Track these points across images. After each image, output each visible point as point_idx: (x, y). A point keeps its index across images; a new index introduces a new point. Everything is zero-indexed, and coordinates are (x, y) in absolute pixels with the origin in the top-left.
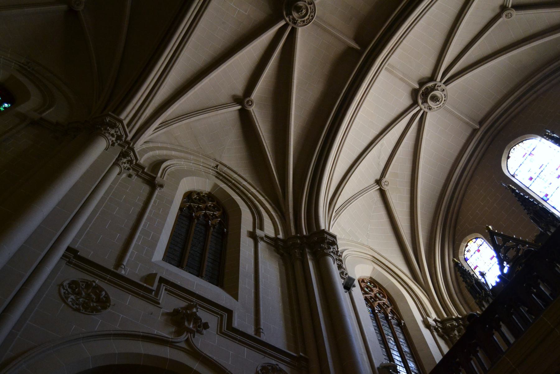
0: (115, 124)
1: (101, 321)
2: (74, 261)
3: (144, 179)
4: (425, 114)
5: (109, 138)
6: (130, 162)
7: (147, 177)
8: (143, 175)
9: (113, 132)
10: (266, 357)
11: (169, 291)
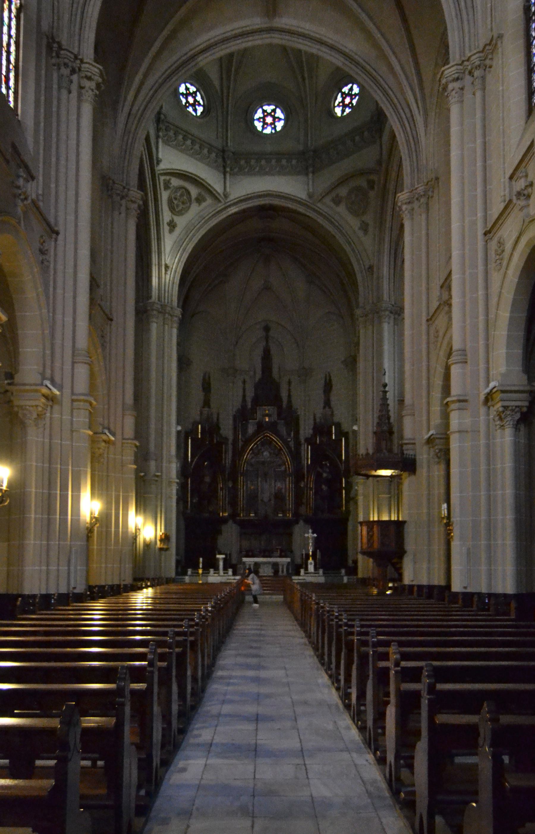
2: (491, 235)
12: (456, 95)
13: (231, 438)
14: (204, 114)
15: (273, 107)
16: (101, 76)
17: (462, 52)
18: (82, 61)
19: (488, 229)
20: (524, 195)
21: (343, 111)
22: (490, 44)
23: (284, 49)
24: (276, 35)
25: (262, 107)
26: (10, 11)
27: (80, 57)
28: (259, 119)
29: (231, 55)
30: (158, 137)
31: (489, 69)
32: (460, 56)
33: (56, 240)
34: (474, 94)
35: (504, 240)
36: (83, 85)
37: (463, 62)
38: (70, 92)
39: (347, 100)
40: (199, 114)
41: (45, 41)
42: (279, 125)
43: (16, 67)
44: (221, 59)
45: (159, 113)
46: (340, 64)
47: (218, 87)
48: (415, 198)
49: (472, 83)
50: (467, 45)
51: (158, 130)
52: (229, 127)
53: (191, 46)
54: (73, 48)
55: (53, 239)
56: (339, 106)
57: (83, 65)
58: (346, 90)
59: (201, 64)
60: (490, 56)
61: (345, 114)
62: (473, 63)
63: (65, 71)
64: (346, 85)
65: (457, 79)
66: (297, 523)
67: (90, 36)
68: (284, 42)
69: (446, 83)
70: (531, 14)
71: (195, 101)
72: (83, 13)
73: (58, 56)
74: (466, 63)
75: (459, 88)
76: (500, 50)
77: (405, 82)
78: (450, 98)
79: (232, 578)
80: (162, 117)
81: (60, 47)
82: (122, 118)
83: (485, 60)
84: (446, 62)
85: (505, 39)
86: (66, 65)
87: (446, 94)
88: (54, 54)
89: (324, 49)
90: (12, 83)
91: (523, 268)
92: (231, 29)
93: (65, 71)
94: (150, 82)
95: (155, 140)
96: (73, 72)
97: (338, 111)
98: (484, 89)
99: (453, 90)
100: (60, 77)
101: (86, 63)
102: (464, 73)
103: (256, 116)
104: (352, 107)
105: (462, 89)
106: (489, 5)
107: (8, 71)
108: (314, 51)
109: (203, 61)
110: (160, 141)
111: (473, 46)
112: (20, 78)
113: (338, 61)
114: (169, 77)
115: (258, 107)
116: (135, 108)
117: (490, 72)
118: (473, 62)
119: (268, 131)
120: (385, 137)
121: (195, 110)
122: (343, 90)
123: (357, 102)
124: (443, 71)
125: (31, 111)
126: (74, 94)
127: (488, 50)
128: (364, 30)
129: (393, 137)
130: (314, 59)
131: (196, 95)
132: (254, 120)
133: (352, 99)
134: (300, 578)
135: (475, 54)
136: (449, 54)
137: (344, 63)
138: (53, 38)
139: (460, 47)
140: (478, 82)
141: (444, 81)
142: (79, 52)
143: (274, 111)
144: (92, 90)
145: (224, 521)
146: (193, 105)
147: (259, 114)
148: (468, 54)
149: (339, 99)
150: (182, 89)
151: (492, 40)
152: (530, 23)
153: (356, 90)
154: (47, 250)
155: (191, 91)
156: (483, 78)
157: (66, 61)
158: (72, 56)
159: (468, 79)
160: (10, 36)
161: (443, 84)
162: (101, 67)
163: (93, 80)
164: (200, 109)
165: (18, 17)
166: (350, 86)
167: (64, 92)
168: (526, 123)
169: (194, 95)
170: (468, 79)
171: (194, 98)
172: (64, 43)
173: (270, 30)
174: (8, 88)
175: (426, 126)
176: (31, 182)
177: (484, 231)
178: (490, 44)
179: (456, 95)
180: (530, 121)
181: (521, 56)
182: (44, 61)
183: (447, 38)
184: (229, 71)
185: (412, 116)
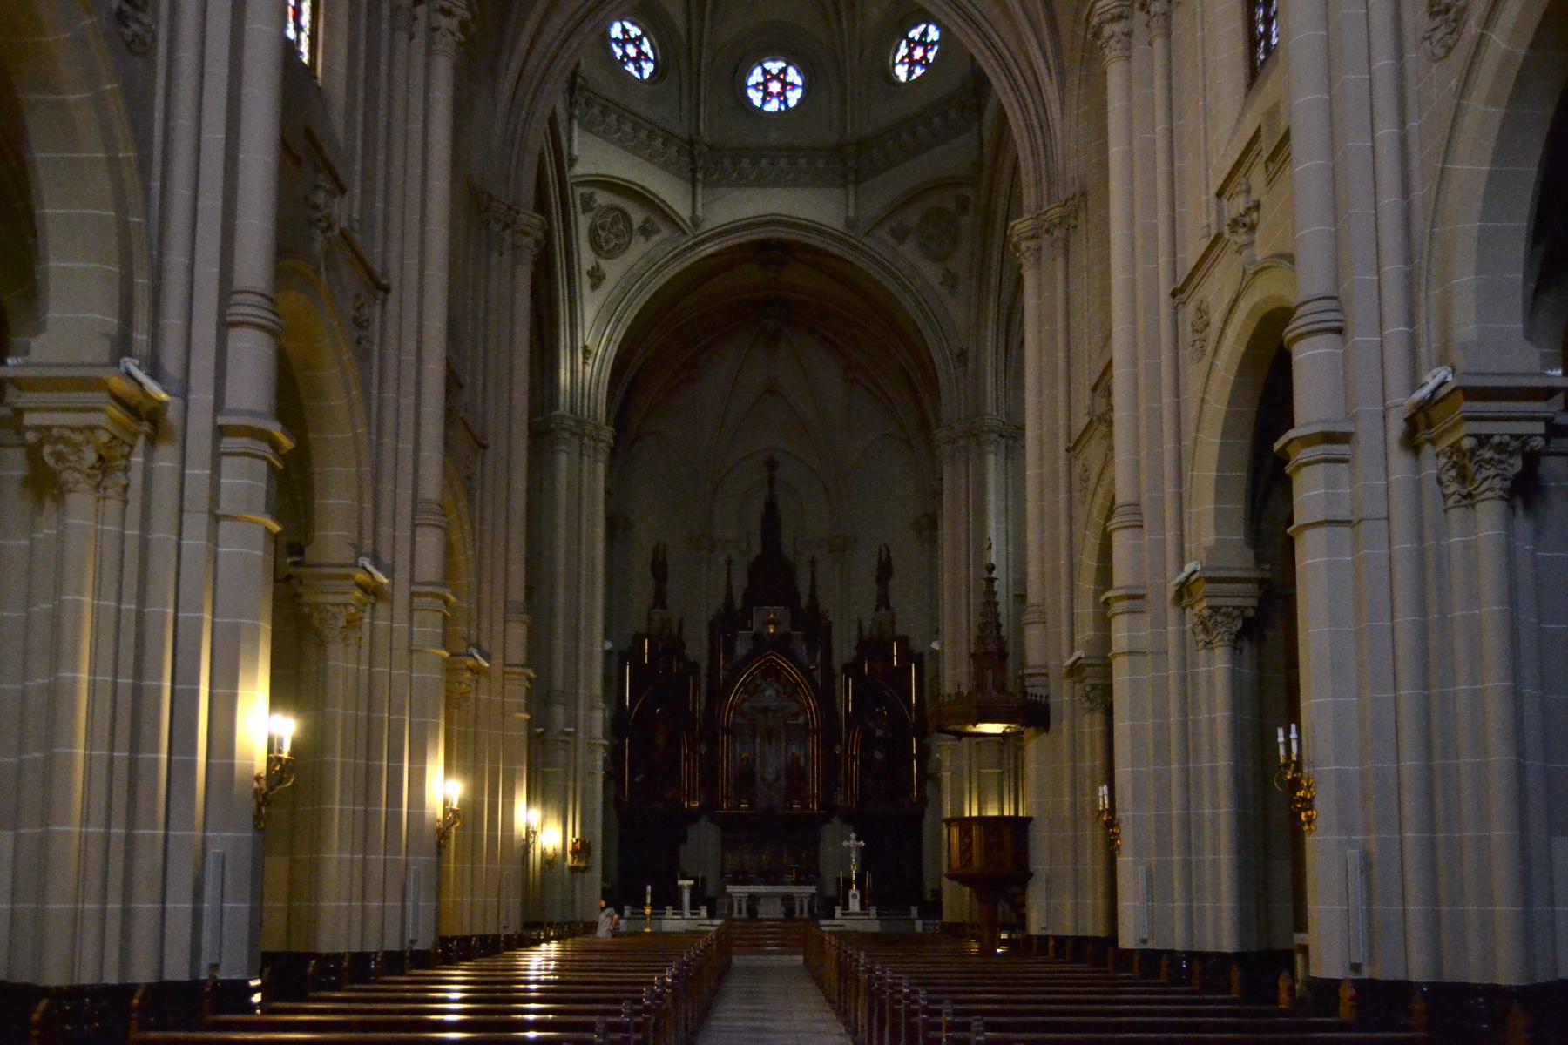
2: (1185, 296)
13: (704, 664)
15: (781, 65)
20: (1245, 225)
21: (910, 72)
22: (1073, 199)
25: (761, 64)
28: (756, 86)
30: (571, 118)
33: (384, 303)
34: (1150, 44)
36: (436, 25)
38: (412, 37)
39: (918, 53)
40: (646, 76)
42: (794, 97)
45: (574, 74)
47: (683, 32)
49: (1147, 25)
51: (572, 104)
55: (378, 302)
58: (915, 34)
61: (914, 77)
64: (916, 26)
66: (828, 820)
69: (1100, 24)
71: (640, 52)
78: (1107, 50)
79: (708, 922)
82: (506, 87)
87: (1099, 43)
90: (305, 19)
96: (507, 226)
97: (901, 72)
99: (1111, 37)
103: (752, 81)
105: (1129, 35)
112: (322, 10)
119: (773, 106)
120: (989, 116)
121: (640, 69)
125: (341, 70)
129: (1002, 118)
131: (641, 42)
133: (926, 51)
134: (836, 922)
140: (1158, 23)
141: (1095, 21)
143: (784, 71)
145: (693, 816)
147: (756, 76)
149: (903, 50)
150: (616, 31)
153: (934, 34)
155: (633, 36)
156: (1067, 241)
161: (1094, 27)
164: (648, 68)
166: (922, 28)
167: (401, 38)
168: (1246, 96)
169: (637, 41)
174: (299, 28)
185: (1037, 82)
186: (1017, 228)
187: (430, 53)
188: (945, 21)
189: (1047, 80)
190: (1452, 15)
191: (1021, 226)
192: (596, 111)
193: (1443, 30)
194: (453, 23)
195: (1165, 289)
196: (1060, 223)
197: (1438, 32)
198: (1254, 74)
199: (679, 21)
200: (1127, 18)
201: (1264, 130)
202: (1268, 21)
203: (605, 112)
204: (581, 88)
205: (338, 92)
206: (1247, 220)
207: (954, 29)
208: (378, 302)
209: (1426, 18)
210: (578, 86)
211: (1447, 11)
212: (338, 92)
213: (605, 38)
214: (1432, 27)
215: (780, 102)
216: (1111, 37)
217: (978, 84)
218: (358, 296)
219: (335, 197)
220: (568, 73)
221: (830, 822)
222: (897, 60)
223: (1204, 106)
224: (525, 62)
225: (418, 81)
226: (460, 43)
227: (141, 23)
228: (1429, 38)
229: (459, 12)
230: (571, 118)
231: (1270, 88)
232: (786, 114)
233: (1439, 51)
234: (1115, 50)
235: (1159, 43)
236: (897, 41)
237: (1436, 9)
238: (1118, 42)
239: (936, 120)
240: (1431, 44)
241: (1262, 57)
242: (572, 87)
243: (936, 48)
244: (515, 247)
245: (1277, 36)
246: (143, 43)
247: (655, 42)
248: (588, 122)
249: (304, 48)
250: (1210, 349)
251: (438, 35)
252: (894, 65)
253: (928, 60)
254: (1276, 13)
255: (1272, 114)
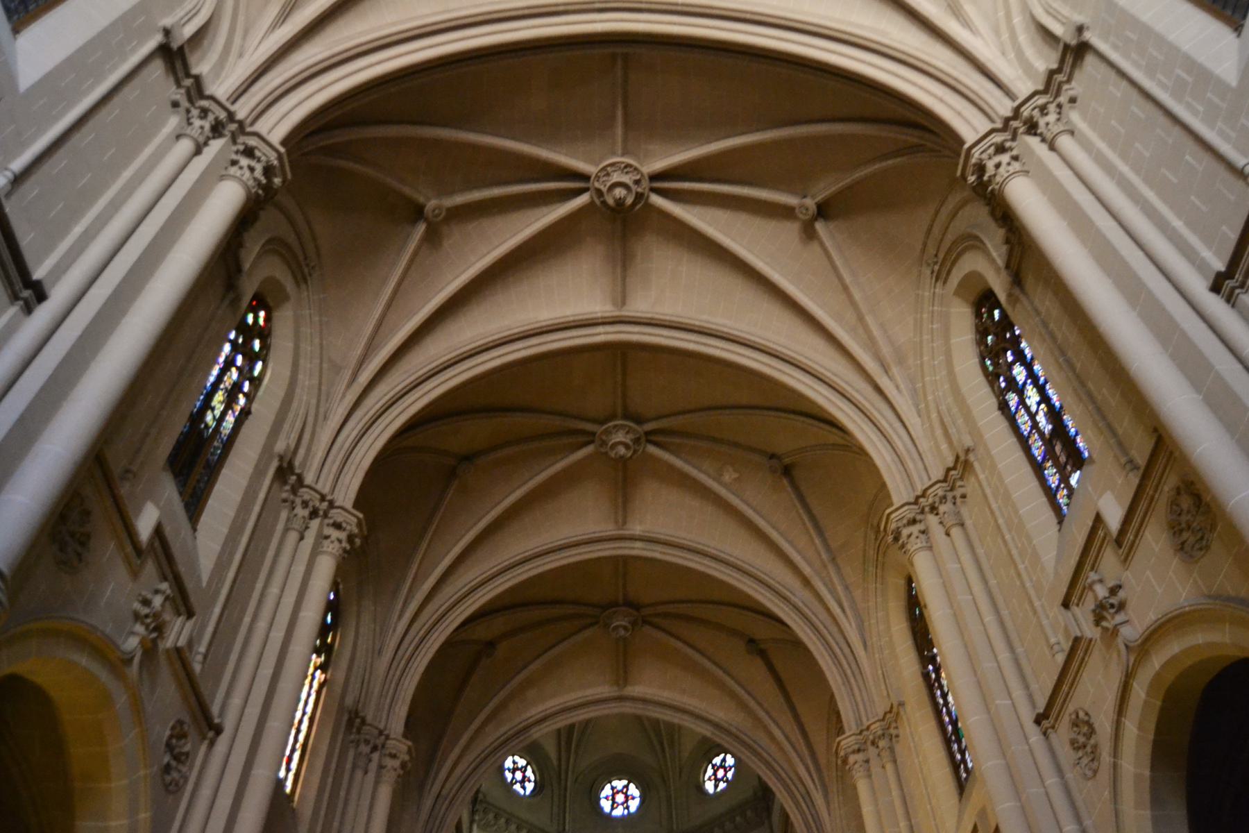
0: (975, 165)
1: (1209, 95)
2: (1051, 720)
3: (1074, 66)
4: (232, 100)
5: (1006, 175)
6: (1043, 109)
7: (1069, 60)
8: (1067, 69)
9: (990, 165)
10: (1135, 480)
11: (1080, 600)
12: (861, 769)
14: (538, 789)
15: (625, 782)
16: (359, 524)
17: (859, 720)
18: (387, 737)
19: (1041, 711)
20: (1112, 606)
21: (716, 786)
22: (954, 468)
23: (638, 718)
24: (628, 704)
25: (610, 782)
26: (311, 687)
27: (386, 732)
28: (607, 798)
29: (572, 727)
30: (472, 822)
31: (897, 739)
32: (857, 725)
33: (212, 744)
34: (883, 767)
35: (1087, 714)
36: (384, 764)
37: (918, 498)
38: (366, 772)
39: (721, 773)
40: (528, 792)
41: (346, 718)
42: (634, 805)
43: (304, 746)
44: (559, 731)
45: (478, 792)
46: (708, 734)
47: (555, 763)
48: (869, 743)
49: (879, 755)
50: (863, 713)
51: (473, 812)
52: (568, 809)
53: (524, 716)
54: (380, 722)
55: (206, 742)
56: (709, 779)
57: (389, 742)
58: (717, 760)
59: (536, 736)
60: (894, 725)
61: (719, 789)
62: (875, 733)
63: (365, 749)
64: (718, 755)
65: (859, 751)
67: (402, 710)
68: (639, 712)
69: (846, 755)
70: (932, 682)
71: (524, 777)
72: (397, 685)
73: (359, 732)
74: (921, 500)
75: (863, 761)
76: (904, 718)
77: (793, 755)
78: (854, 772)
80: (481, 796)
81: (363, 722)
82: (428, 803)
83: (888, 728)
84: (840, 731)
85: (908, 708)
86: (367, 742)
87: (847, 767)
88: (354, 730)
89: (686, 717)
90: (294, 765)
91: (1153, 752)
92: (576, 697)
93: (365, 749)
94: (470, 757)
95: (468, 825)
96: (375, 749)
97: (709, 787)
98: (895, 761)
99: (856, 763)
100: (357, 756)
101: (394, 739)
102: (865, 742)
103: (603, 794)
104: (727, 781)
105: (867, 761)
106: (880, 672)
107: (293, 750)
108: (676, 721)
109: (536, 734)
110: (475, 827)
111: (870, 716)
112: (307, 757)
113: (706, 731)
114: (496, 749)
115: (605, 783)
116: (448, 786)
117: (898, 742)
118: (874, 731)
119: (618, 812)
120: (776, 817)
121: (524, 788)
122: (714, 762)
123: (734, 775)
124: (839, 743)
125: (312, 794)
126: (371, 775)
127: (890, 717)
128: (733, 695)
129: (786, 817)
130: (674, 731)
131: (526, 770)
132: (600, 799)
133: (726, 772)
135: (874, 723)
136: (841, 722)
137: (713, 734)
138: (291, 464)
139: (853, 711)
140: (885, 754)
141: (842, 753)
142: (385, 728)
143: (627, 787)
144: (395, 770)
146: (522, 782)
147: (607, 791)
148: (866, 724)
149: (710, 771)
150: (508, 763)
151: (892, 707)
152: (933, 690)
153: (730, 761)
154: (187, 754)
155: (520, 766)
156: (892, 749)
157: (367, 737)
158: (318, 496)
159: (872, 751)
160: (304, 713)
161: (842, 757)
162: (361, 516)
163: (344, 530)
164: (530, 787)
165: (319, 693)
166: (722, 756)
167: (293, 536)
168: (960, 800)
169: (523, 770)
170: (872, 751)
171: (524, 772)
172: (369, 719)
173: (621, 699)
174: (288, 770)
175: (828, 804)
176: (181, 619)
177: (1034, 716)
178: (890, 712)
179: (861, 769)
180: (963, 799)
181: (932, 724)
182: (340, 737)
183: (836, 705)
184: (569, 743)
185: (808, 793)
186: (842, 743)
187: (315, 553)
188: (735, 751)
189: (847, 625)
190: (1089, 749)
191: (847, 741)
192: (491, 816)
193: (1085, 761)
194: (396, 763)
195: (1028, 717)
196: (883, 735)
197: (1083, 760)
198: (961, 787)
199: (553, 754)
200: (864, 750)
201: (978, 825)
202: (963, 753)
203: (496, 817)
204: (481, 801)
205: (306, 813)
206: (1113, 600)
207: (743, 757)
208: (206, 742)
209: (1072, 751)
210: (479, 799)
211: (1085, 747)
212: (306, 813)
213: (501, 769)
214: (1078, 757)
215: (624, 809)
216: (856, 763)
217: (764, 796)
218: (180, 723)
219: (179, 615)
220: (472, 794)
221: (1093, 724)
222: (706, 779)
223: (932, 809)
224: (442, 787)
225: (366, 803)
226: (345, 550)
227: (180, 771)
228: (1078, 764)
229: (348, 528)
230: (472, 822)
231: (976, 796)
232: (627, 820)
233: (1090, 773)
234: (860, 772)
235: (889, 767)
236: (705, 765)
237: (1076, 745)
238: (861, 766)
239: (738, 819)
240: (1081, 767)
241: (964, 775)
242: (475, 801)
243: (733, 769)
244: (381, 767)
245: (971, 761)
246: (177, 785)
247: (535, 769)
248: (485, 824)
249: (289, 784)
250: (1106, 757)
251: (384, 771)
252: (704, 782)
253: (727, 779)
254: (966, 746)
255: (983, 813)
